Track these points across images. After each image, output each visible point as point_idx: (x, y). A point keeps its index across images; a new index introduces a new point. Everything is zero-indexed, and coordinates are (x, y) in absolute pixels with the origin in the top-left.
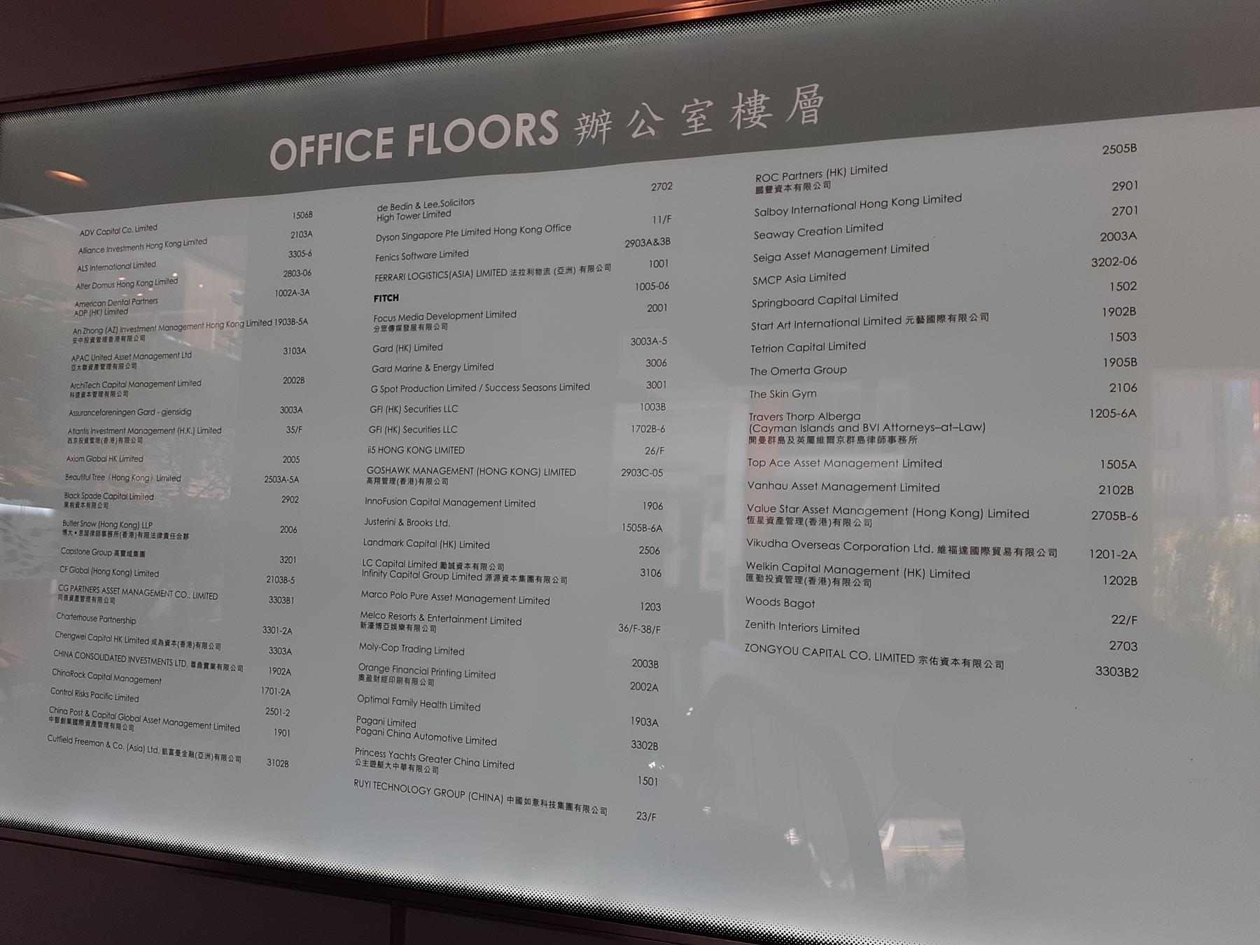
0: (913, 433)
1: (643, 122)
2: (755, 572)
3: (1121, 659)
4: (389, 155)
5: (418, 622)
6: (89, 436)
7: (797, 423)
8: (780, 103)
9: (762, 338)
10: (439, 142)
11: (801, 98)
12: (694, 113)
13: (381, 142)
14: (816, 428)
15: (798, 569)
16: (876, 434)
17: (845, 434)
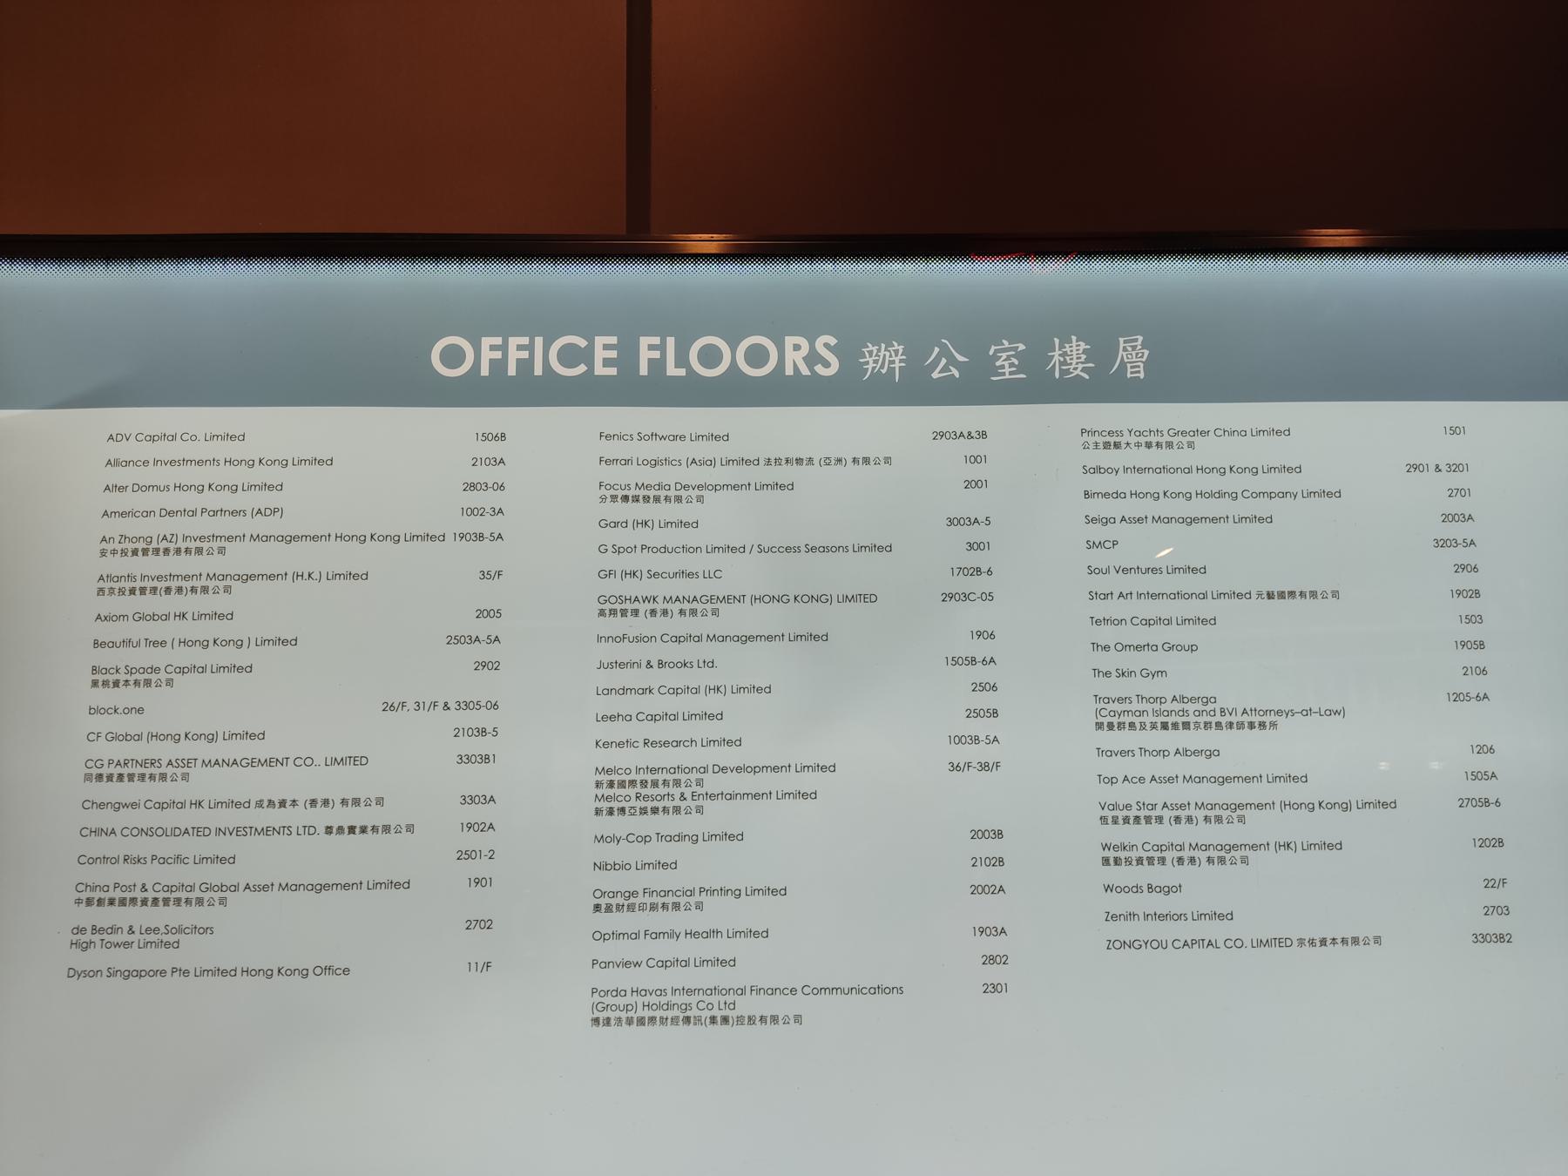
0: (1273, 718)
1: (944, 361)
2: (1111, 854)
3: (1496, 924)
4: (613, 371)
5: (677, 803)
6: (138, 584)
7: (1149, 707)
8: (1102, 353)
9: (1101, 609)
10: (682, 360)
11: (1125, 349)
12: (1004, 355)
13: (600, 354)
14: (1170, 713)
15: (1160, 848)
16: (1234, 719)
17: (1202, 719)
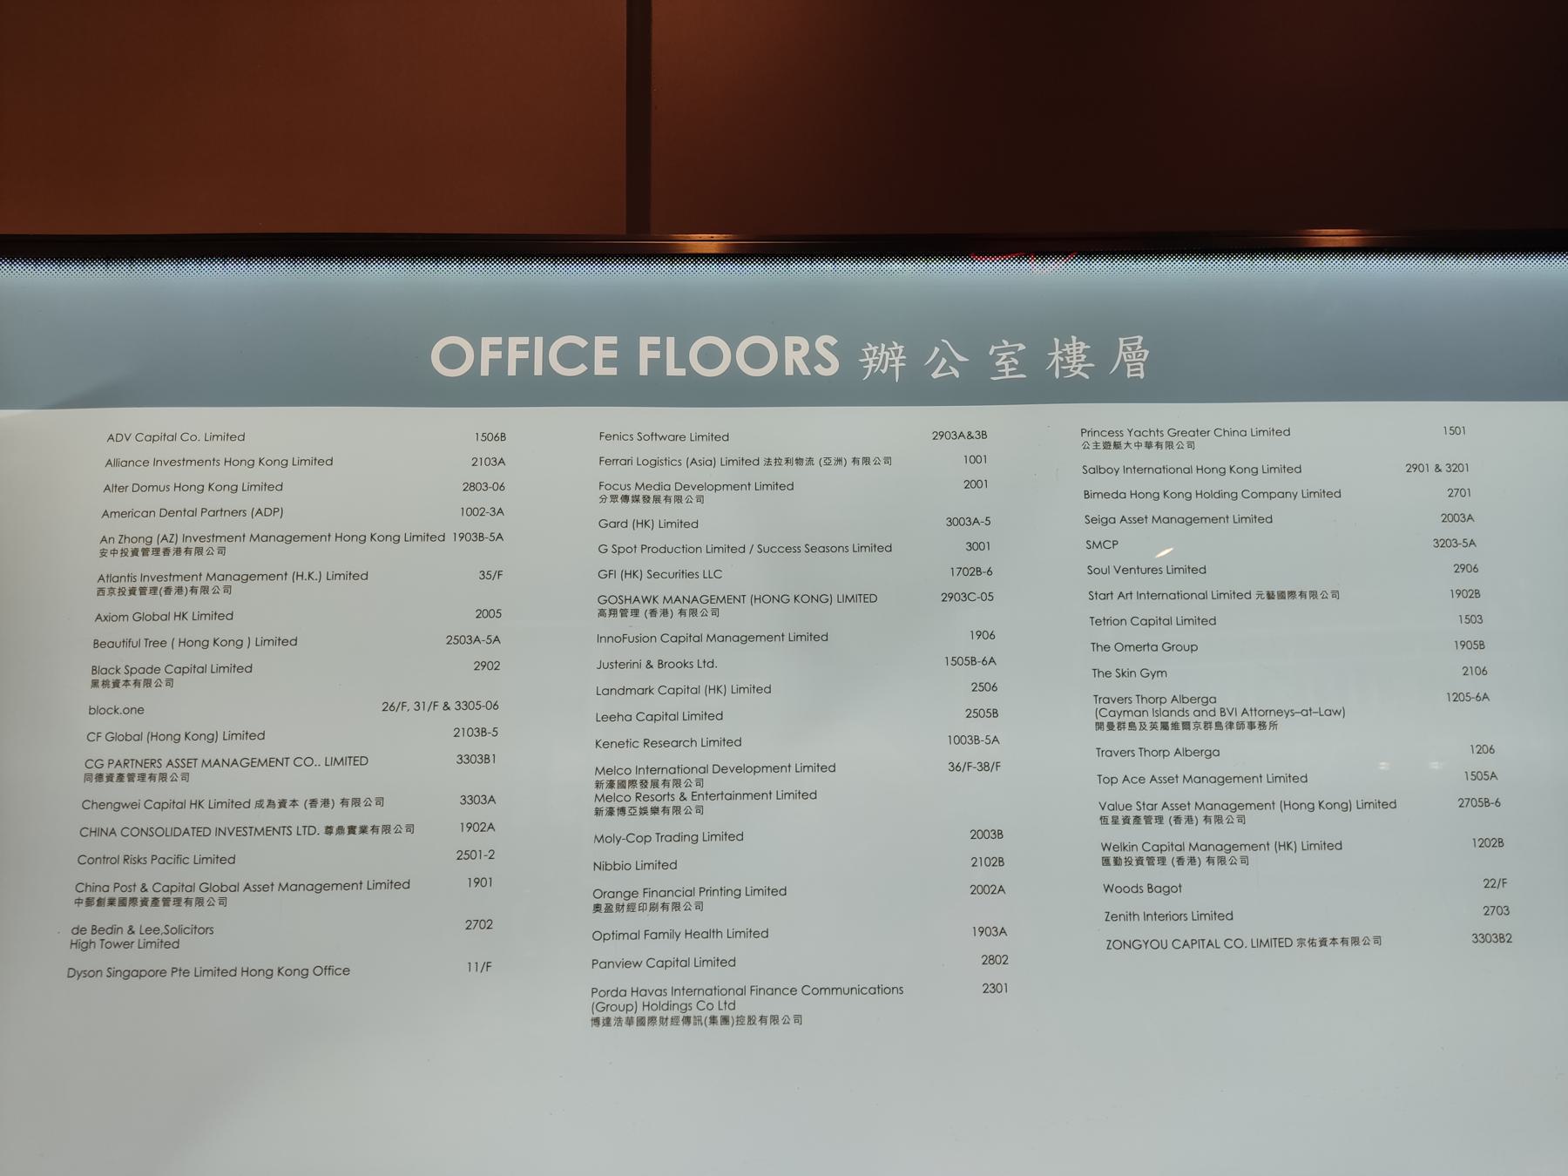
0: (1273, 718)
1: (944, 361)
2: (1111, 854)
3: (1496, 924)
4: (613, 371)
5: (677, 803)
6: (138, 584)
7: (1149, 707)
8: (1102, 353)
9: (1101, 609)
10: (682, 360)
11: (1125, 349)
12: (1004, 355)
13: (600, 354)
14: (1170, 713)
15: (1160, 848)
16: (1234, 719)
17: (1202, 719)
